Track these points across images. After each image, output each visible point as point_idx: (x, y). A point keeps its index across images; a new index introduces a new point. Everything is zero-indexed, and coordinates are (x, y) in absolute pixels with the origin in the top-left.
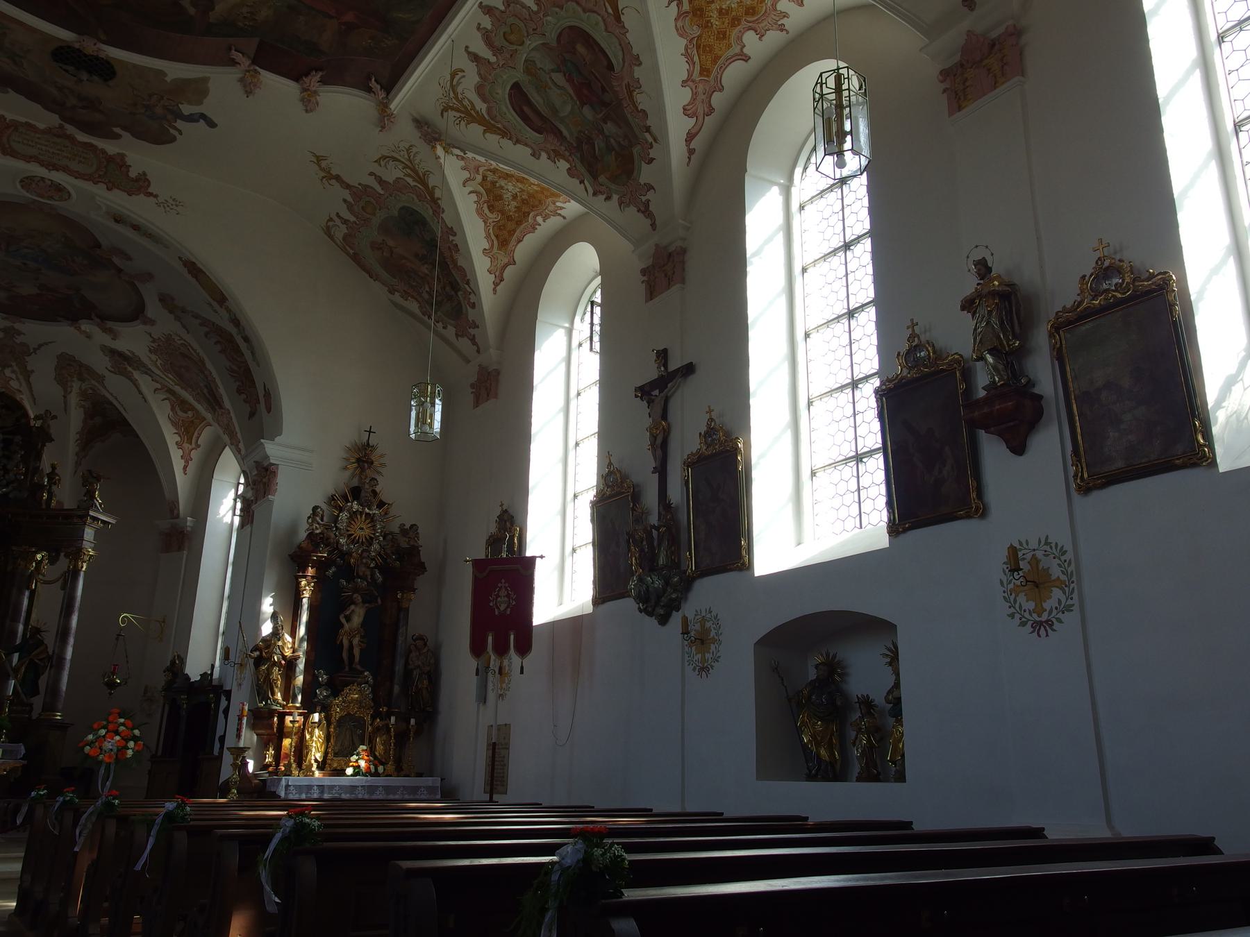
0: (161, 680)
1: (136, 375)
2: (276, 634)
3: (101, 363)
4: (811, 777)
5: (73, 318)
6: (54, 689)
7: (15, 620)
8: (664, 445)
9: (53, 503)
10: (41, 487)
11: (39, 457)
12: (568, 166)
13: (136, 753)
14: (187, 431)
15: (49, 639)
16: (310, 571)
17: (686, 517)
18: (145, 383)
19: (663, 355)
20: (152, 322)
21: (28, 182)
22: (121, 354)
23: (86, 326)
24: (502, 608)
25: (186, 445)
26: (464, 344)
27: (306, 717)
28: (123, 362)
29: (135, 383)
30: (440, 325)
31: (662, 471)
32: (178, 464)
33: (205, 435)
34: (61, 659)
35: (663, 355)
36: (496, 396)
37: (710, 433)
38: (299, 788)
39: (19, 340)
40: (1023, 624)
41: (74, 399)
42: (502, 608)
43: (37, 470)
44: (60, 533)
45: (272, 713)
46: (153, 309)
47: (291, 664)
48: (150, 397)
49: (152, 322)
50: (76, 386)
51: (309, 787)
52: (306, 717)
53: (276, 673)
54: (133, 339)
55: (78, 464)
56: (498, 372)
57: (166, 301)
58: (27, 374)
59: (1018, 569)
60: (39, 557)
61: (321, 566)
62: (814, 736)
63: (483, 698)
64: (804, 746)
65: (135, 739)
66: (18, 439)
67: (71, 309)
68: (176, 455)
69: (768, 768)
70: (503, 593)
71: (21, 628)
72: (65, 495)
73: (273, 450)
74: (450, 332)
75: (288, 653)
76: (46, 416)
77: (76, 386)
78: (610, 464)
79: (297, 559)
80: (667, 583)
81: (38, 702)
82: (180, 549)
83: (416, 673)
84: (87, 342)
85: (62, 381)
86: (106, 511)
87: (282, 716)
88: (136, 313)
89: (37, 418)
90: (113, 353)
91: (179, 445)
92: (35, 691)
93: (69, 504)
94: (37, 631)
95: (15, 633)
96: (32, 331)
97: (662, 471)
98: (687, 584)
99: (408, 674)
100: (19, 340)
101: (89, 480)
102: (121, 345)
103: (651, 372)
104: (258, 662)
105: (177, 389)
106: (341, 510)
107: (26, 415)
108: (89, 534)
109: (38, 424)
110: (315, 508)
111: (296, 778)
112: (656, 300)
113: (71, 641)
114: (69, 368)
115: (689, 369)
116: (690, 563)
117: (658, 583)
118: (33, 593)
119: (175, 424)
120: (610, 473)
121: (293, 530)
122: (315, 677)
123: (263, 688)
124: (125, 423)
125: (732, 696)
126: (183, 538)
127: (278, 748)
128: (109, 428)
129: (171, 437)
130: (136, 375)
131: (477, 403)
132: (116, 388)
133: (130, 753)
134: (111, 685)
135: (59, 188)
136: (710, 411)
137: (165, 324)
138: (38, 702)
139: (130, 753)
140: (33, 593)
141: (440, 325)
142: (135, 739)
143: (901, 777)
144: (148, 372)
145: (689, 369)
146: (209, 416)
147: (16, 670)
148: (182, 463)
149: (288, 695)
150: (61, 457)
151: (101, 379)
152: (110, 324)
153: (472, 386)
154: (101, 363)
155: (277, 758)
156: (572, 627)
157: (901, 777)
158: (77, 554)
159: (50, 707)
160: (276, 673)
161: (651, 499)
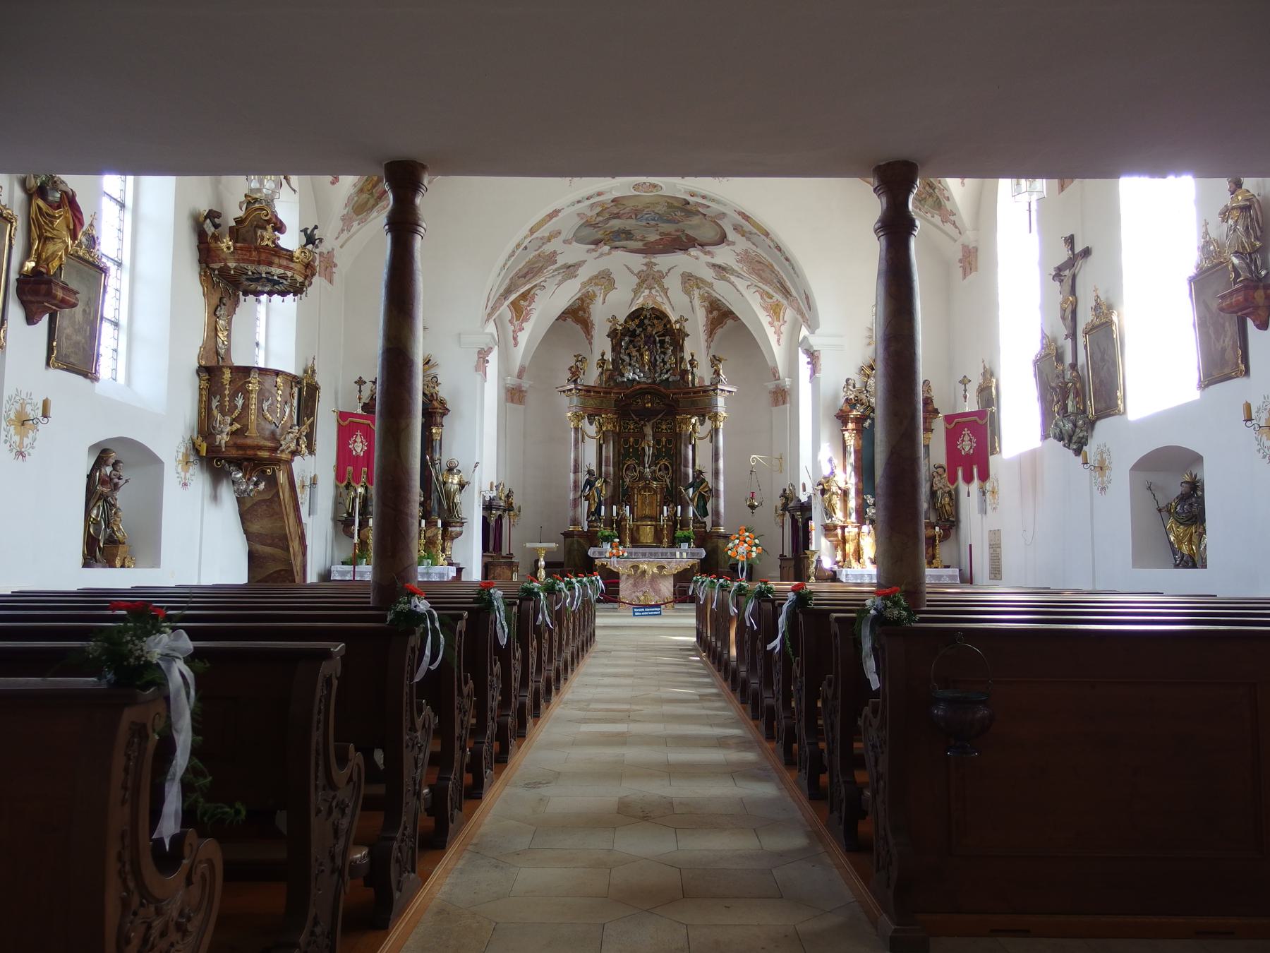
0: (779, 502)
1: (733, 278)
2: (832, 473)
3: (708, 274)
4: (1177, 566)
5: (684, 249)
6: (716, 513)
7: (686, 466)
8: (1074, 312)
9: (696, 381)
10: (686, 372)
11: (682, 350)
12: (438, 749)
13: (758, 554)
14: (775, 311)
15: (708, 477)
16: (851, 426)
17: (1088, 374)
18: (741, 284)
19: (1070, 241)
20: (733, 243)
21: (636, 187)
22: (720, 267)
23: (693, 252)
24: (967, 449)
25: (776, 323)
26: (948, 227)
27: (860, 528)
28: (721, 269)
29: (732, 283)
30: (929, 215)
31: (1073, 335)
32: (773, 339)
33: (789, 314)
34: (717, 491)
35: (1070, 241)
36: (976, 269)
37: (1097, 307)
38: (855, 576)
39: (656, 269)
40: (1264, 457)
41: (697, 302)
42: (967, 449)
43: (682, 358)
44: (698, 402)
45: (835, 527)
46: (732, 235)
47: (845, 493)
48: (744, 292)
49: (733, 243)
50: (696, 292)
51: (862, 576)
52: (860, 528)
53: (837, 502)
54: (723, 255)
55: (709, 347)
56: (976, 249)
57: (736, 228)
58: (665, 291)
59: (1250, 420)
60: (693, 421)
61: (859, 421)
62: (1176, 537)
63: (984, 511)
64: (1171, 543)
65: (756, 545)
66: (667, 339)
67: (681, 243)
68: (770, 331)
69: (1141, 558)
70: (967, 438)
71: (690, 471)
72: (703, 374)
73: (816, 342)
74: (937, 220)
75: (842, 485)
76: (682, 320)
77: (696, 292)
78: (1207, 233)
79: (842, 418)
80: (1075, 426)
81: (708, 520)
82: (784, 403)
83: (939, 493)
84: (693, 262)
85: (687, 291)
86: (730, 383)
87: (843, 528)
88: (722, 239)
89: (677, 322)
90: (714, 265)
91: (771, 324)
92: (706, 514)
93: (707, 383)
94: (701, 472)
95: (687, 475)
96: (663, 261)
97: (1073, 335)
98: (1091, 425)
99: (933, 494)
100: (656, 269)
101: (715, 361)
102: (718, 260)
103: (1063, 255)
104: (823, 492)
105: (760, 285)
106: (869, 377)
107: (669, 321)
108: (721, 401)
109: (678, 326)
110: (848, 380)
111: (856, 568)
112: (1067, 190)
113: (722, 478)
114: (690, 281)
115: (1087, 252)
116: (1091, 412)
117: (1069, 426)
118: (694, 447)
119: (765, 309)
120: (1207, 243)
121: (836, 397)
122: (864, 500)
123: (829, 511)
124: (732, 313)
125: (1117, 510)
126: (782, 396)
127: (844, 550)
128: (720, 315)
129: (765, 319)
130: (733, 278)
131: (965, 276)
132: (722, 291)
133: (754, 555)
134: (752, 507)
135: (655, 186)
136: (1095, 290)
137: (742, 244)
138: (708, 520)
139: (754, 555)
140: (694, 447)
141: (929, 215)
142: (756, 545)
143: (1204, 566)
144: (739, 276)
145: (1087, 252)
146: (785, 302)
147: (692, 500)
148: (776, 337)
149: (847, 514)
150: (696, 346)
151: (711, 285)
152: (708, 248)
153: (960, 261)
154: (708, 274)
155: (844, 556)
156: (1033, 458)
157: (1204, 566)
158: (715, 417)
159: (716, 524)
160: (837, 502)
161: (1068, 359)
